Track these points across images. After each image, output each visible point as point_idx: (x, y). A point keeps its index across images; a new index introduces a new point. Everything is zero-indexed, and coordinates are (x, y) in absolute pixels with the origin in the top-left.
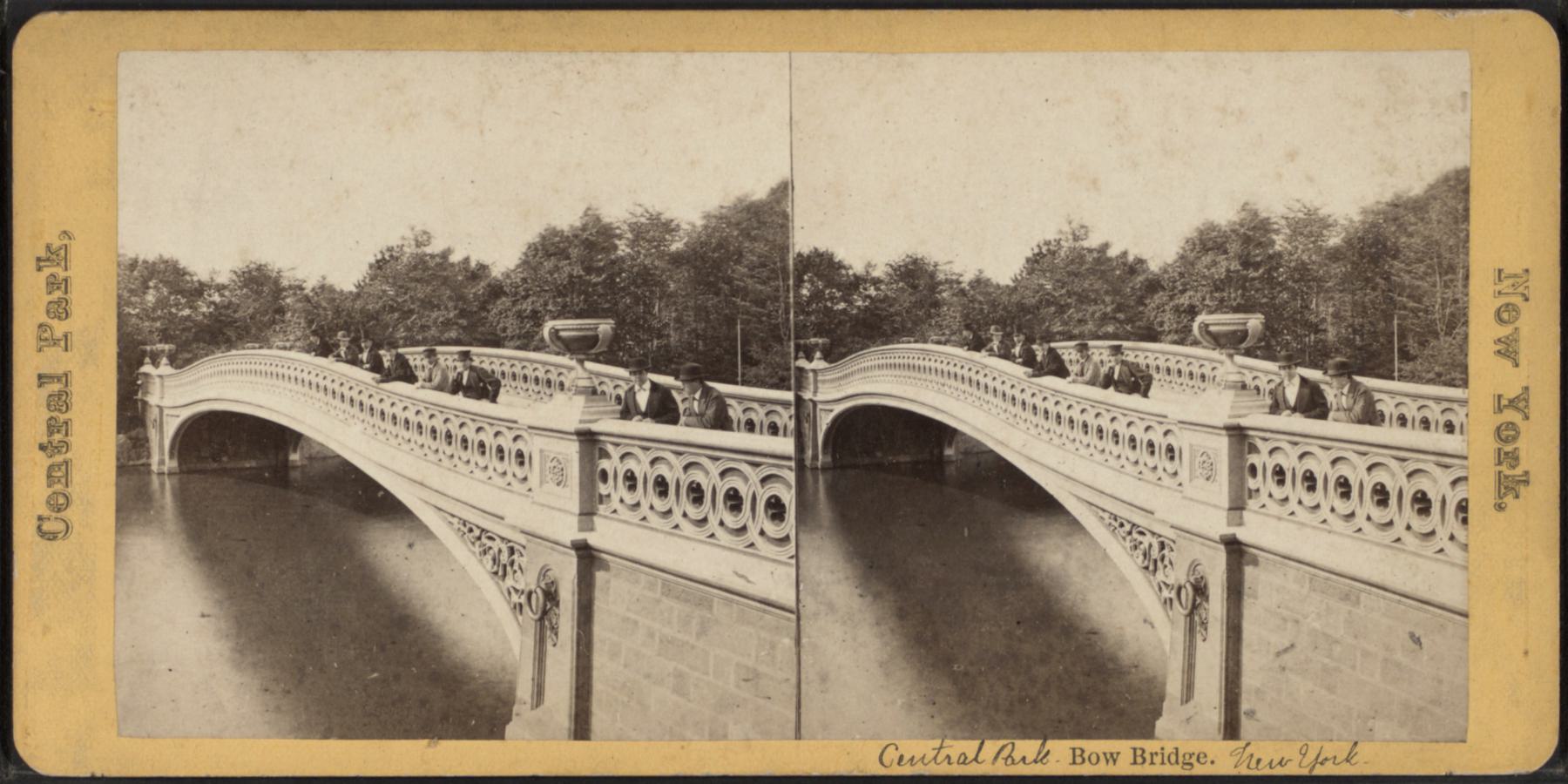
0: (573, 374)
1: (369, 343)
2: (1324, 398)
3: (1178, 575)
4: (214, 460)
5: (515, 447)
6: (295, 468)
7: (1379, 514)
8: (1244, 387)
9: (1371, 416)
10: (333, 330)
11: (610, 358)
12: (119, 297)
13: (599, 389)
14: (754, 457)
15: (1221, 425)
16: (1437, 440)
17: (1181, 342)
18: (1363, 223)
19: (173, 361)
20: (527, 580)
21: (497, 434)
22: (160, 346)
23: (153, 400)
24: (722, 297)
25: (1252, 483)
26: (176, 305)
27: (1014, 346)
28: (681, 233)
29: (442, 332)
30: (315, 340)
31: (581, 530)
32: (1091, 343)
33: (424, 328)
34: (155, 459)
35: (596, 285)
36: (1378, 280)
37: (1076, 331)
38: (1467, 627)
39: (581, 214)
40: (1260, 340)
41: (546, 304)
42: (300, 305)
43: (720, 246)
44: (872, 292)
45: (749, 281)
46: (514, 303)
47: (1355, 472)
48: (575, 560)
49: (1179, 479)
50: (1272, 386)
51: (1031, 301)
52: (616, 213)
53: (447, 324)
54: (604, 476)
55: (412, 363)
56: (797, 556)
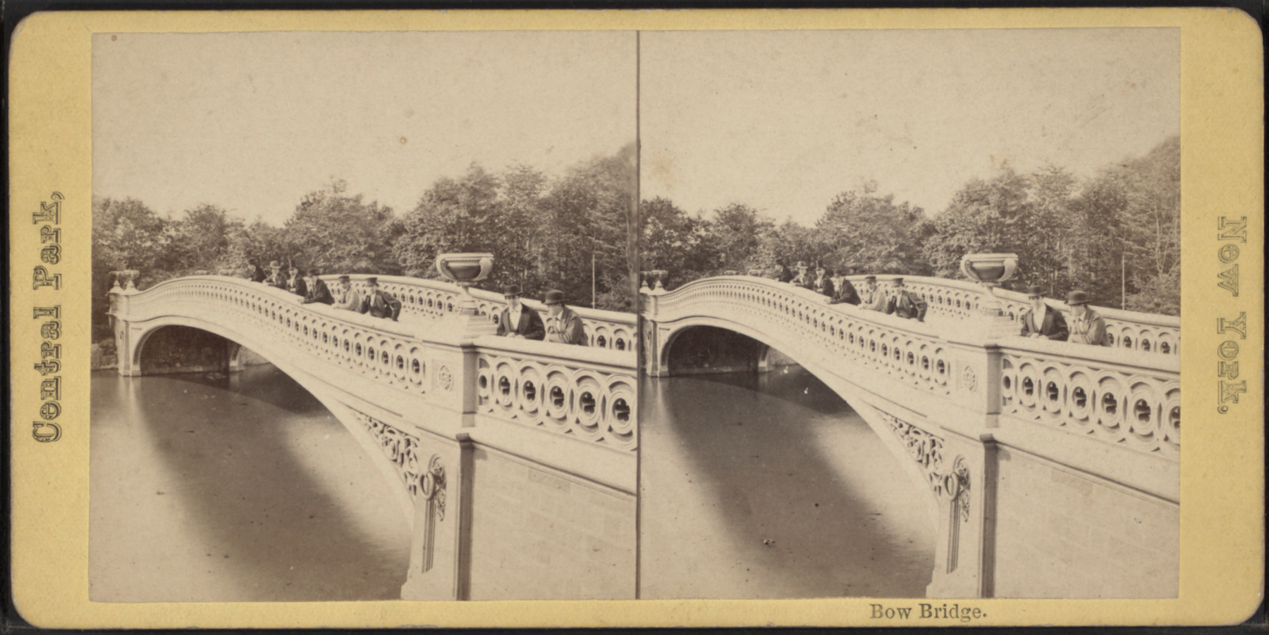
1: (296, 271)
2: (1064, 323)
3: (946, 468)
4: (170, 365)
6: (234, 373)
8: (1001, 314)
9: (579, 338)
11: (489, 284)
12: (94, 230)
13: (481, 310)
14: (606, 368)
15: (457, 343)
16: (1156, 358)
17: (951, 276)
18: (568, 179)
19: (137, 283)
22: (655, 272)
23: (120, 315)
24: (1110, 237)
25: (482, 392)
27: (816, 278)
28: (548, 183)
29: (354, 263)
30: (252, 268)
32: (878, 277)
35: (479, 225)
36: (1110, 227)
37: (866, 267)
38: (1178, 511)
40: (1014, 275)
41: (438, 241)
42: (240, 239)
43: (579, 195)
44: (703, 233)
45: (1132, 225)
46: (944, 239)
47: (567, 383)
49: (423, 388)
50: (1024, 312)
51: (829, 241)
53: (358, 256)
55: (330, 288)
56: (638, 449)
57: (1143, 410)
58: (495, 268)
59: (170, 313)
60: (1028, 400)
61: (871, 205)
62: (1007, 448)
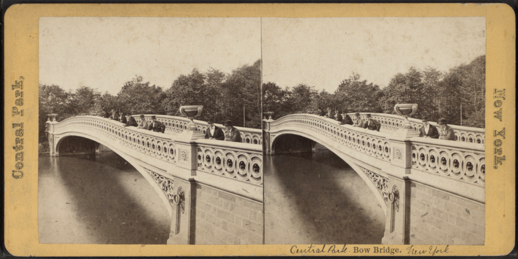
0: (189, 124)
1: (122, 113)
3: (389, 190)
4: (71, 152)
5: (170, 148)
6: (97, 154)
7: (455, 170)
8: (411, 128)
9: (453, 137)
10: (110, 109)
11: (202, 118)
12: (39, 98)
13: (198, 129)
14: (249, 151)
15: (403, 140)
16: (475, 145)
17: (390, 113)
18: (450, 74)
19: (57, 119)
20: (174, 192)
21: (164, 143)
22: (53, 114)
23: (51, 132)
24: (239, 98)
25: (414, 160)
26: (58, 101)
27: (335, 114)
28: (225, 77)
29: (146, 110)
31: (192, 175)
33: (140, 108)
34: (51, 152)
35: (197, 94)
36: (455, 92)
37: (356, 110)
38: (485, 207)
39: (192, 71)
40: (416, 112)
41: (180, 100)
43: (238, 81)
44: (288, 96)
45: (248, 93)
46: (170, 100)
47: (448, 156)
48: (190, 185)
49: (389, 158)
50: (420, 127)
51: (341, 99)
52: (204, 70)
53: (148, 107)
54: (200, 157)
55: (136, 120)
56: (263, 184)
57: (470, 166)
58: (204, 112)
59: (82, 132)
61: (357, 85)
62: (200, 184)
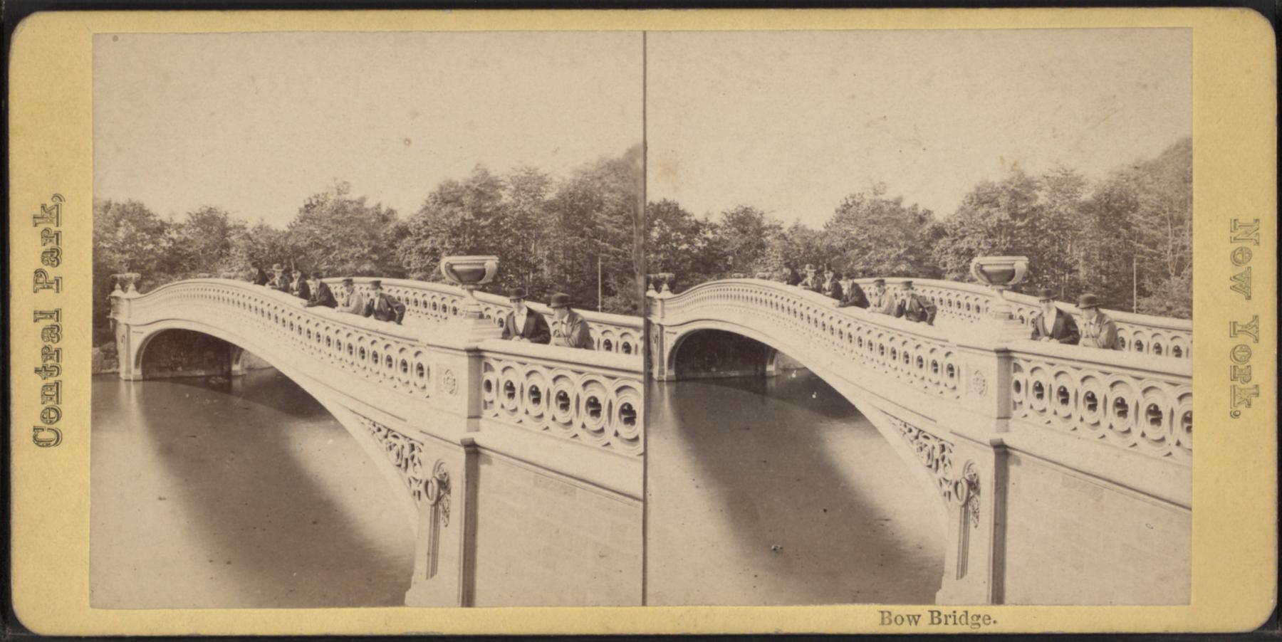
1: (299, 274)
2: (1075, 326)
3: (425, 472)
4: (171, 369)
6: (237, 377)
8: (1011, 317)
9: (585, 342)
10: (269, 263)
11: (495, 287)
12: (95, 233)
13: (485, 314)
14: (612, 372)
15: (462, 346)
16: (1168, 362)
17: (960, 279)
18: (574, 181)
19: (138, 286)
22: (661, 275)
23: (122, 319)
24: (1121, 240)
25: (487, 396)
26: (142, 241)
27: (824, 281)
28: (554, 185)
29: (358, 265)
30: (254, 271)
33: (343, 261)
35: (484, 227)
36: (1121, 230)
37: (875, 270)
38: (1190, 517)
40: (1025, 278)
41: (443, 243)
42: (777, 242)
43: (585, 197)
44: (710, 235)
45: (1144, 227)
46: (953, 242)
47: (573, 387)
49: (428, 391)
50: (1034, 316)
51: (838, 243)
53: (362, 259)
55: (333, 291)
57: (1155, 414)
58: (500, 271)
60: (1039, 404)
